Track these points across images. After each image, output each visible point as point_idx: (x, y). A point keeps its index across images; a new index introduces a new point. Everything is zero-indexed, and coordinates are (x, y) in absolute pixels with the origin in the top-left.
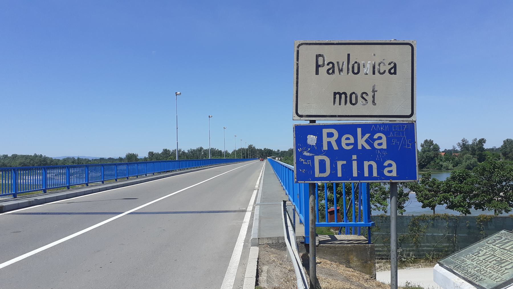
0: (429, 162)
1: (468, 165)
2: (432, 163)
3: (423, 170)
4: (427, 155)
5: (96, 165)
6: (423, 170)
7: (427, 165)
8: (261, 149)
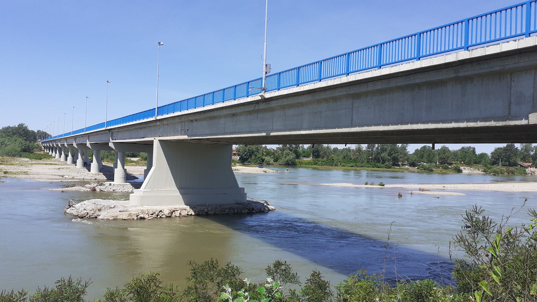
0: (251, 156)
1: (287, 161)
2: (253, 157)
3: (245, 163)
4: (250, 148)
5: (194, 135)
6: (245, 163)
7: (248, 159)
8: (34, 131)
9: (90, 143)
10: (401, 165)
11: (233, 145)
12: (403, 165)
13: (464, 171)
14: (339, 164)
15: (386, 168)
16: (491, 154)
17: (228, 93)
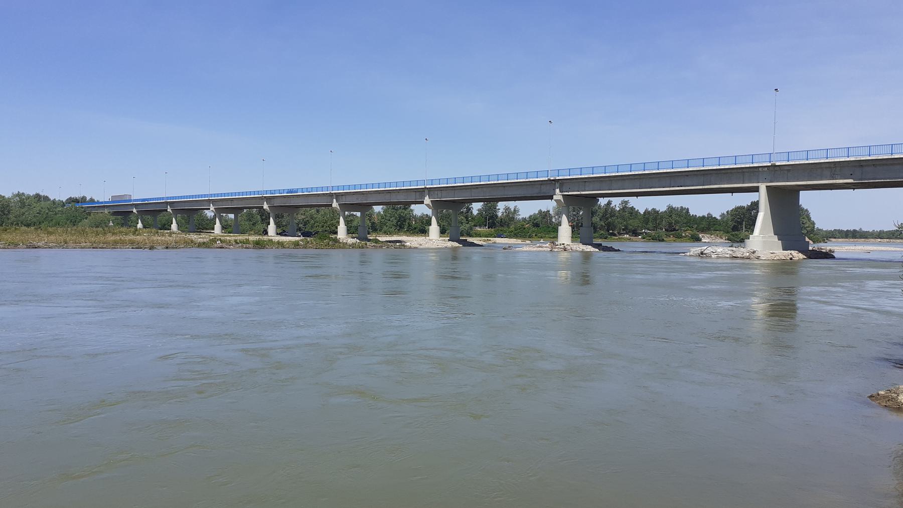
9: (431, 201)
11: (800, 192)
12: (620, 234)
14: (534, 235)
15: (601, 238)
16: (478, 210)
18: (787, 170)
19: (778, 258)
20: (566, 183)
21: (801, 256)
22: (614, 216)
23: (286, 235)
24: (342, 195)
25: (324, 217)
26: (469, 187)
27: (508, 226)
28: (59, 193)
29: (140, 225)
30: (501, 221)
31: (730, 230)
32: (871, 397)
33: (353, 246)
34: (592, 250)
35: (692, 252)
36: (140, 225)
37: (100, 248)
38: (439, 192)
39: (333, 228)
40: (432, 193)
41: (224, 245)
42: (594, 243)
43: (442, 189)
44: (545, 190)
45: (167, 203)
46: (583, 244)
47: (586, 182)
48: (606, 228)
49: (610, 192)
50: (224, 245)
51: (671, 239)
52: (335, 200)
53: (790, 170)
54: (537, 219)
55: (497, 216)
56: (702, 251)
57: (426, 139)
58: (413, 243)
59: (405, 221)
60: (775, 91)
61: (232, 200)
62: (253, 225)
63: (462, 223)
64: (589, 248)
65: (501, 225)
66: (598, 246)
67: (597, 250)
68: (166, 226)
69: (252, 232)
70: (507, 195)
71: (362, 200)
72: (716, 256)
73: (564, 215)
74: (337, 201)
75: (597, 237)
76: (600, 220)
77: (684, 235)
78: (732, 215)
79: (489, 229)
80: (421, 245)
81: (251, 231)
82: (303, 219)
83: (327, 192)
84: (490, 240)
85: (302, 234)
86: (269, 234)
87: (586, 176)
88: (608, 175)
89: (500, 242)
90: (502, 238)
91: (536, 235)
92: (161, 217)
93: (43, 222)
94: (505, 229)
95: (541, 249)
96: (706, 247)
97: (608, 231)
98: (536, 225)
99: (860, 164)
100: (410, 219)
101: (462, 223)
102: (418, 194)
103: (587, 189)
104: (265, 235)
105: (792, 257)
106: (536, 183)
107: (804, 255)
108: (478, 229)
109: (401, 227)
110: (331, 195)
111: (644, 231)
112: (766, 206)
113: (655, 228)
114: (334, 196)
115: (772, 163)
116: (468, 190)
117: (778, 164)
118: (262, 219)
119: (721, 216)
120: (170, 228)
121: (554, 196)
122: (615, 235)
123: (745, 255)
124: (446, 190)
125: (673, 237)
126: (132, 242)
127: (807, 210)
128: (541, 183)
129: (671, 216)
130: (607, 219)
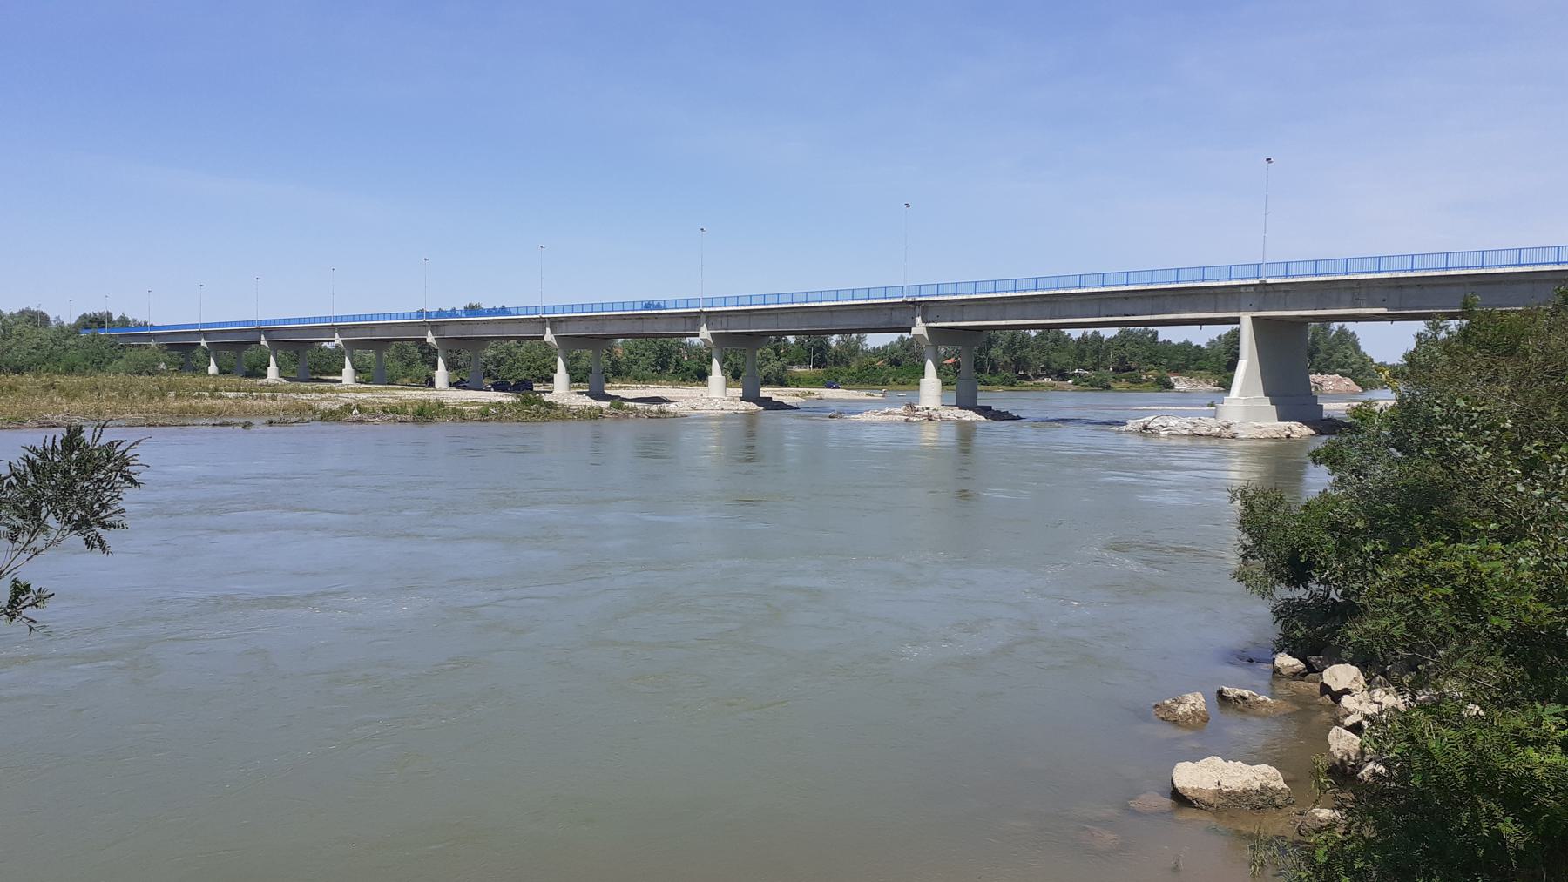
9: (1252, 317)
10: (1032, 377)
12: (1037, 377)
13: (1177, 387)
14: (891, 379)
15: (1003, 384)
17: (238, 324)
18: (1285, 291)
19: (1267, 435)
20: (932, 307)
21: (1307, 430)
22: (1026, 346)
23: (465, 388)
24: (562, 321)
25: (530, 353)
26: (773, 312)
27: (848, 365)
28: (65, 310)
29: (213, 369)
30: (836, 356)
31: (1223, 369)
32: (1156, 706)
33: (580, 415)
34: (974, 419)
35: (1130, 425)
36: (213, 369)
37: (160, 425)
38: (724, 320)
39: (547, 371)
40: (712, 320)
41: (365, 416)
42: (978, 404)
43: (729, 314)
44: (898, 317)
45: (259, 330)
46: (960, 409)
47: (963, 306)
48: (1013, 366)
49: (1003, 323)
50: (365, 416)
51: (1122, 385)
52: (548, 330)
53: (1288, 291)
54: (896, 352)
55: (828, 346)
56: (1146, 423)
57: (702, 229)
58: (681, 406)
59: (670, 356)
60: (1267, 162)
61: (372, 326)
62: (407, 365)
63: (768, 360)
64: (970, 416)
65: (835, 362)
66: (985, 411)
67: (983, 418)
68: (258, 371)
69: (406, 381)
70: (837, 326)
71: (595, 330)
72: (1167, 432)
73: (929, 360)
74: (552, 332)
75: (999, 383)
76: (1004, 353)
77: (1144, 377)
78: (1226, 344)
79: (816, 370)
80: (694, 409)
81: (405, 377)
82: (494, 357)
83: (535, 316)
84: (813, 394)
85: (493, 386)
86: (437, 386)
87: (965, 297)
88: (999, 295)
89: (830, 396)
90: (834, 388)
91: (894, 380)
92: (251, 354)
93: (45, 364)
94: (842, 369)
95: (890, 417)
96: (1152, 418)
97: (1017, 373)
98: (895, 362)
99: (1398, 284)
100: (678, 352)
101: (768, 360)
102: (688, 321)
103: (965, 318)
104: (429, 387)
105: (1289, 433)
106: (884, 306)
107: (1311, 428)
108: (796, 369)
109: (663, 366)
110: (542, 321)
111: (1076, 371)
112: (1250, 347)
113: (1095, 367)
114: (548, 324)
115: (1260, 279)
116: (772, 317)
117: (1270, 281)
118: (423, 355)
119: (1208, 344)
120: (265, 372)
121: (913, 329)
122: (1027, 378)
123: (1213, 431)
124: (736, 316)
125: (1127, 381)
126: (210, 411)
127: (1353, 334)
128: (891, 306)
129: (1123, 345)
130: (1015, 351)
